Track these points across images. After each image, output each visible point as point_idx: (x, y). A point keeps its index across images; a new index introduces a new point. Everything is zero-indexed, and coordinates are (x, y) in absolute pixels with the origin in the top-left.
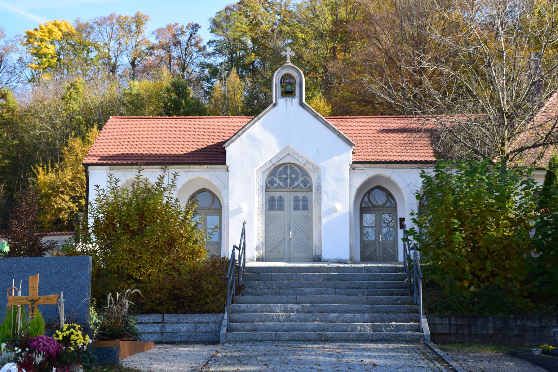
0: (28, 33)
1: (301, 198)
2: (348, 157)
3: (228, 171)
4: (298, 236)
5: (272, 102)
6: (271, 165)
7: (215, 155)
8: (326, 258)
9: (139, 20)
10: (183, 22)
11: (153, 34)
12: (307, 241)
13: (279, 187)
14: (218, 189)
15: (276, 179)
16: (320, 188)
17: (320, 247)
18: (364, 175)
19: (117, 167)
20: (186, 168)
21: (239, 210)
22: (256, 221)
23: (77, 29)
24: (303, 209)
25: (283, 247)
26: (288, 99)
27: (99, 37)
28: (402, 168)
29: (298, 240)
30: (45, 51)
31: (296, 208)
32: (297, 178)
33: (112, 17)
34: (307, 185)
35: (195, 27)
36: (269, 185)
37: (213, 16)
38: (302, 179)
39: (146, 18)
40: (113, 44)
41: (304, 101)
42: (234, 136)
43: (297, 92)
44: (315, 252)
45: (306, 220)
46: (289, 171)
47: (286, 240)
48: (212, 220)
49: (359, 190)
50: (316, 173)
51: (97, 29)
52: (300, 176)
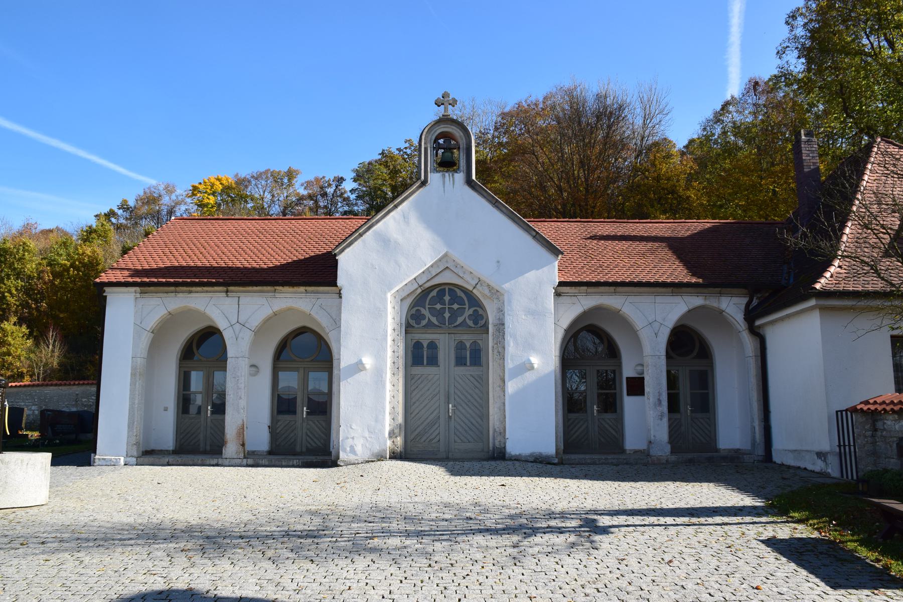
0: (193, 186)
1: (468, 345)
2: (550, 273)
3: (341, 297)
4: (463, 411)
5: (419, 178)
6: (416, 286)
7: (320, 271)
8: (513, 453)
9: (291, 174)
10: (330, 176)
11: (302, 185)
12: (479, 420)
13: (430, 324)
14: (323, 329)
15: (426, 312)
16: (501, 327)
17: (503, 433)
18: (578, 305)
19: (152, 288)
20: (268, 292)
21: (359, 367)
22: (388, 386)
23: (236, 183)
24: (471, 365)
25: (437, 432)
26: (447, 174)
27: (255, 190)
28: (640, 294)
29: (464, 419)
30: (206, 201)
31: (460, 361)
32: (461, 311)
33: (267, 171)
34: (479, 321)
35: (340, 180)
36: (412, 322)
37: (356, 167)
38: (471, 311)
39: (297, 172)
40: (268, 196)
41: (474, 177)
42: (351, 235)
43: (463, 163)
44: (493, 441)
45: (476, 383)
46: (447, 298)
47: (442, 420)
48: (317, 381)
49: (567, 331)
50: (495, 301)
51: (253, 182)
52: (467, 306)
